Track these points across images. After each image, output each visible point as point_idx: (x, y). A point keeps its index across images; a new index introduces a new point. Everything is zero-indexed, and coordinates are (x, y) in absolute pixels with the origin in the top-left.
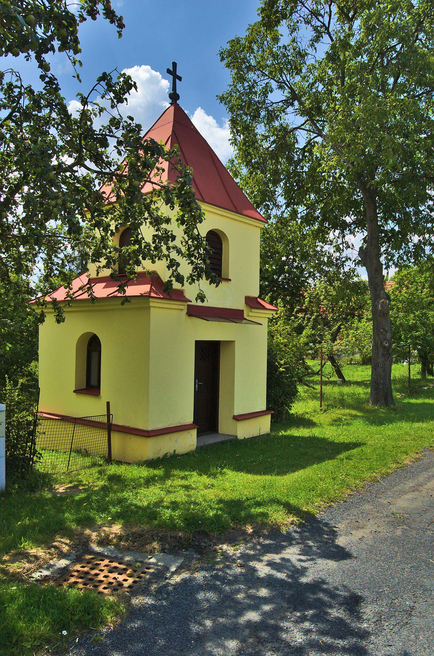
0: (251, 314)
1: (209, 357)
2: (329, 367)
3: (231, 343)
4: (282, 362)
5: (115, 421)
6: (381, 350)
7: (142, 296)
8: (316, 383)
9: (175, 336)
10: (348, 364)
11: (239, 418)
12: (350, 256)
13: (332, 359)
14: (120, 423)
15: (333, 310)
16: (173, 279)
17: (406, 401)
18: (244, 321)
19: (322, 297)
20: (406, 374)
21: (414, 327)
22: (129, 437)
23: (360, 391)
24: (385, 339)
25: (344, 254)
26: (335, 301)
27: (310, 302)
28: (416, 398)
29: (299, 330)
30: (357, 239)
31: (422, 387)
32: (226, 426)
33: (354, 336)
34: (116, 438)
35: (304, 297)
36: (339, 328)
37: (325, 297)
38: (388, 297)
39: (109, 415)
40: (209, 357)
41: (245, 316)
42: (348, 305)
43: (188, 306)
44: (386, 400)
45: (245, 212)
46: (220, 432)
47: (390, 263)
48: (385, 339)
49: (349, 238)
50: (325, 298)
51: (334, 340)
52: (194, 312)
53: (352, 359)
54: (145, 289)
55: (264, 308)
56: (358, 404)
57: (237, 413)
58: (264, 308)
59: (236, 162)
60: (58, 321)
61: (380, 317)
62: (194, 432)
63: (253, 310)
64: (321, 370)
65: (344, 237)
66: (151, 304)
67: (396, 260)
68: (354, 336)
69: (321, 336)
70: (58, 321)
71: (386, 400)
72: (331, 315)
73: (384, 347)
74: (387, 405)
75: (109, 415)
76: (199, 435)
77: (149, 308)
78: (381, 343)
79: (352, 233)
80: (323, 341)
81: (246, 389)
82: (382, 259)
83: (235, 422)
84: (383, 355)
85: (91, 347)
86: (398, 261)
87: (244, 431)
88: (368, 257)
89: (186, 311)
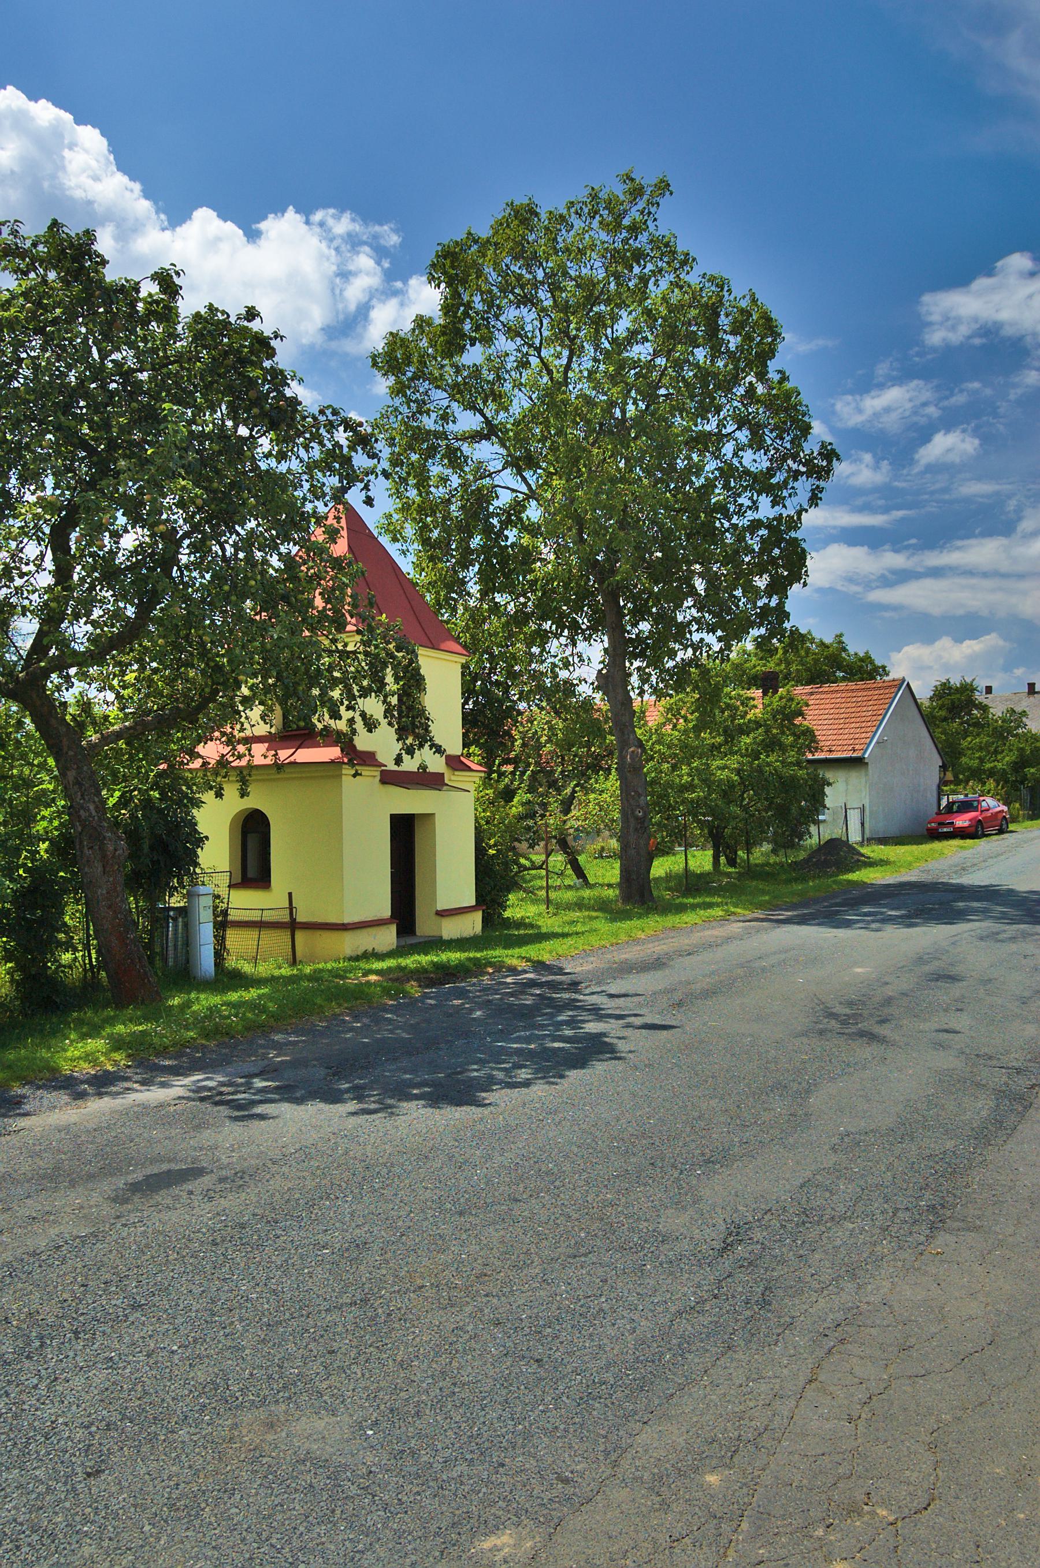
0: (453, 778)
1: (406, 834)
2: (558, 860)
3: (429, 817)
4: (492, 842)
5: (300, 918)
6: (632, 823)
7: (332, 762)
8: (541, 888)
9: (368, 809)
10: (596, 858)
11: (442, 914)
12: (584, 676)
13: (563, 845)
14: (304, 920)
15: (563, 759)
16: (403, 752)
17: (678, 901)
18: (445, 788)
19: (544, 739)
20: (682, 865)
21: (690, 787)
22: (319, 933)
23: (611, 893)
24: (638, 806)
25: (575, 675)
26: (567, 745)
27: (524, 745)
28: (694, 897)
29: (508, 795)
30: (595, 651)
31: (708, 883)
32: (425, 926)
33: (598, 804)
34: (300, 936)
35: (511, 736)
36: (574, 792)
37: (549, 738)
38: (640, 744)
39: (291, 908)
40: (406, 834)
41: (446, 781)
42: (589, 750)
43: (382, 771)
44: (642, 895)
45: (442, 646)
46: (418, 932)
47: (646, 687)
48: (638, 806)
49: (582, 646)
50: (549, 741)
51: (566, 811)
52: (389, 778)
53: (603, 848)
54: (333, 753)
55: (469, 769)
56: (603, 906)
57: (440, 907)
58: (469, 769)
59: (396, 517)
60: (242, 797)
61: (630, 774)
62: (393, 928)
63: (456, 773)
64: (545, 862)
65: (574, 645)
66: (344, 772)
67: (654, 683)
68: (598, 804)
69: (544, 806)
70: (242, 797)
71: (642, 895)
72: (560, 769)
73: (637, 818)
74: (643, 903)
75: (291, 908)
76: (399, 934)
77: (340, 776)
78: (633, 813)
79: (587, 639)
80: (548, 814)
81: (452, 877)
82: (635, 680)
83: (438, 917)
84: (636, 829)
85: (253, 830)
86: (657, 683)
87: (450, 929)
88: (612, 680)
89: (379, 778)
